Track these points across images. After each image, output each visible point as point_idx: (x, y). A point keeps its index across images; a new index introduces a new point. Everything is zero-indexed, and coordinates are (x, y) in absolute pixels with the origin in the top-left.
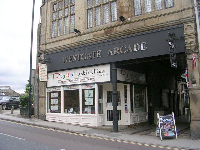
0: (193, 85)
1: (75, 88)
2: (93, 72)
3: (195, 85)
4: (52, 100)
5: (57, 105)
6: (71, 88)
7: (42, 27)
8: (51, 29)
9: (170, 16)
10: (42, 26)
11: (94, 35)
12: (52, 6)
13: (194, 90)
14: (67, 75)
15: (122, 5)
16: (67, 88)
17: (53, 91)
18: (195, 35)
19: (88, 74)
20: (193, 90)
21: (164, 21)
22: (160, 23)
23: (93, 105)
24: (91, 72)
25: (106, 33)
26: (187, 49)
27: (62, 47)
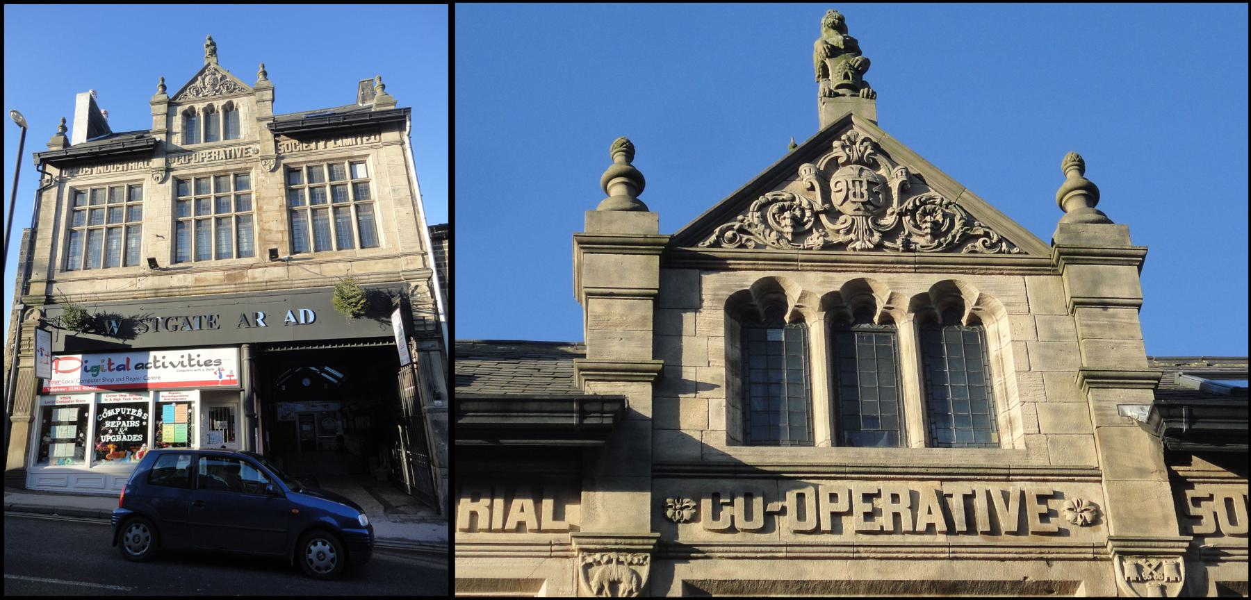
0: (436, 402)
1: (134, 399)
2: (186, 363)
3: (440, 402)
4: (823, 528)
5: (72, 441)
6: (122, 398)
7: (40, 239)
8: (67, 249)
9: (376, 263)
10: (39, 236)
11: (196, 280)
12: (73, 196)
13: (439, 412)
14: (106, 367)
15: (266, 226)
16: (109, 398)
17: (64, 404)
18: (433, 305)
19: (170, 366)
20: (436, 412)
21: (367, 272)
22: (108, 289)
23: (892, 529)
24: (181, 360)
25: (228, 277)
26: (416, 329)
27: (313, 281)
